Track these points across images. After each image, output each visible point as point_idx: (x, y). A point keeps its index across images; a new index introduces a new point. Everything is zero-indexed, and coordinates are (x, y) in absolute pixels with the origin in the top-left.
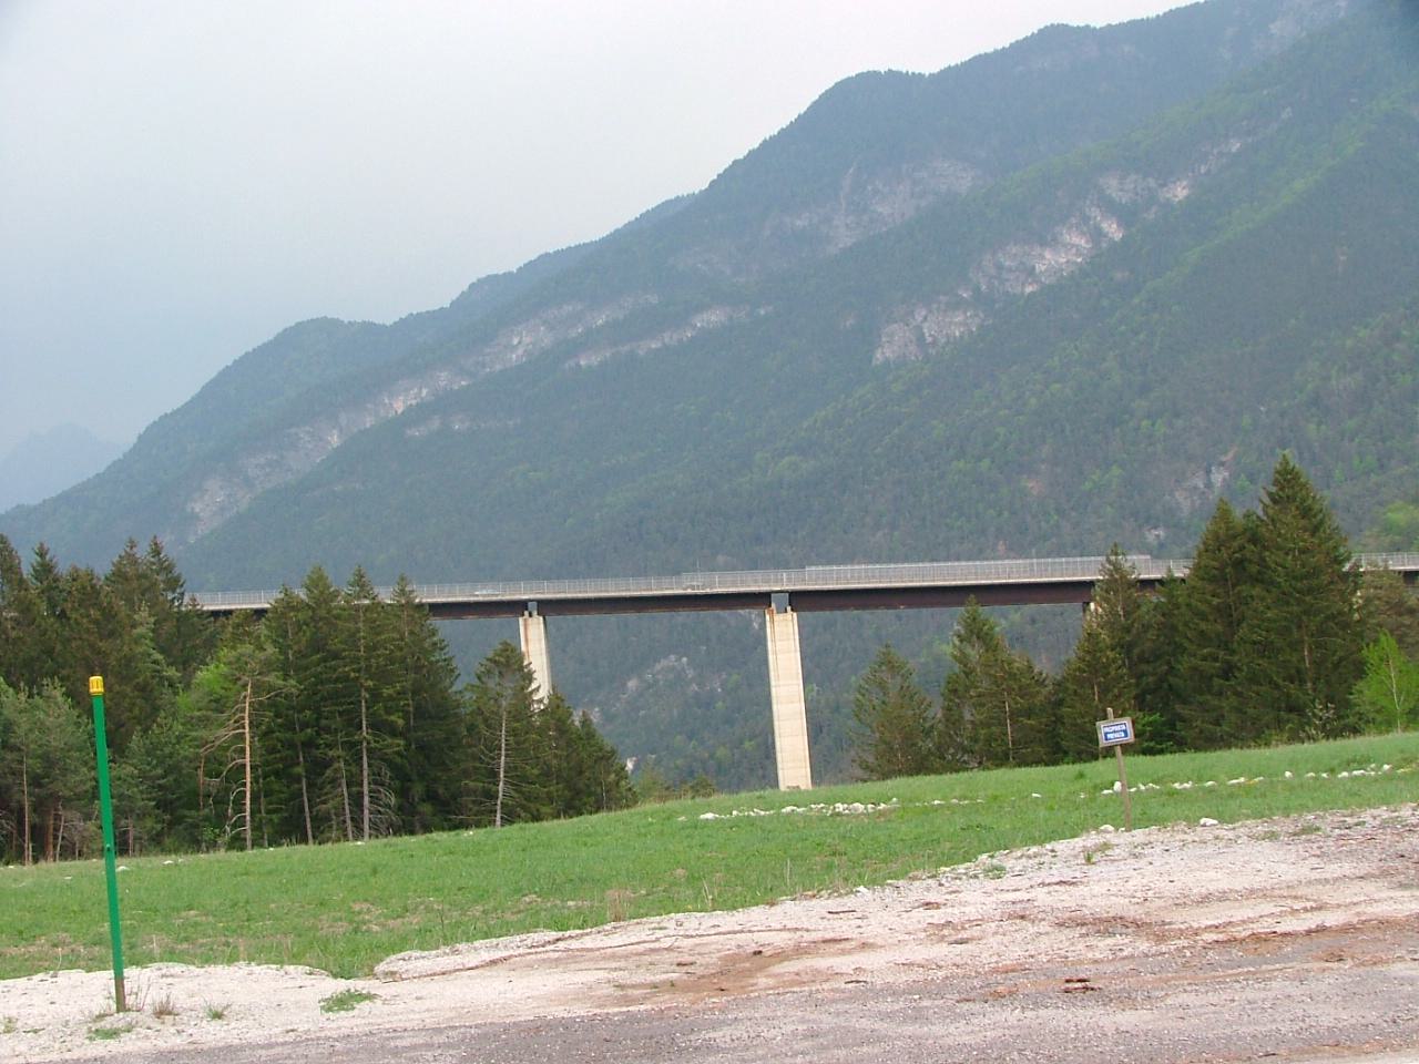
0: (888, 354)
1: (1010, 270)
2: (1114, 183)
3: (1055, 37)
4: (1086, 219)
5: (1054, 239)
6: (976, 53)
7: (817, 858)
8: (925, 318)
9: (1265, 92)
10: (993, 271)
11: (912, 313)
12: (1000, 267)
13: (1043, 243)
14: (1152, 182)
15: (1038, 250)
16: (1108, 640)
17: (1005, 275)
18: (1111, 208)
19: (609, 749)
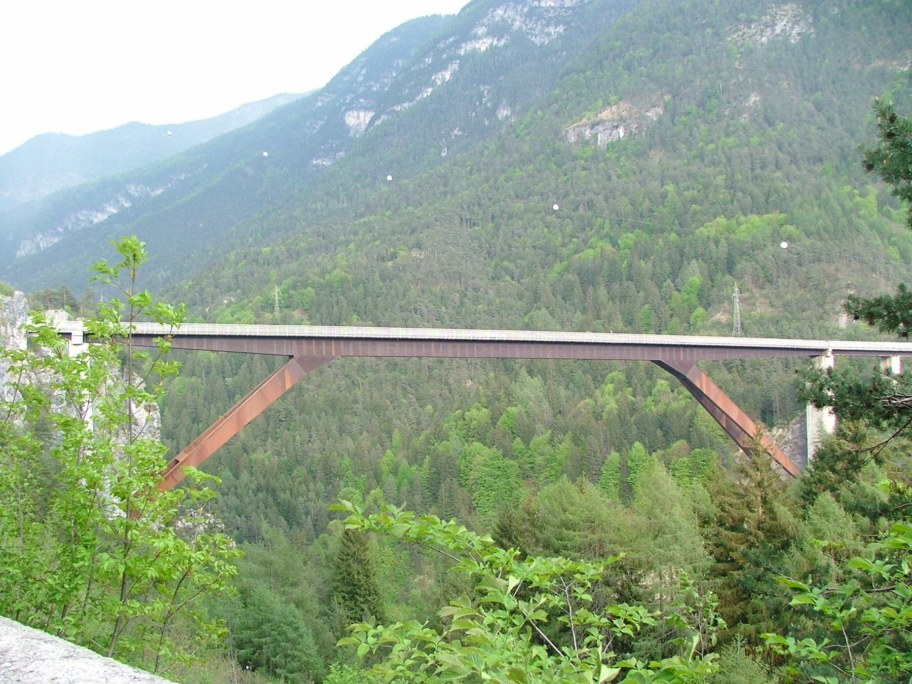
0: (23, 253)
1: (82, 221)
2: (133, 188)
3: (133, 127)
4: (118, 202)
5: (103, 209)
6: (404, 19)
7: (685, 459)
8: (41, 239)
9: (412, 83)
10: (74, 221)
11: (35, 236)
12: (78, 219)
13: (98, 211)
14: (148, 189)
15: (95, 213)
16: (691, 279)
17: (79, 223)
18: (129, 197)
19: (749, 239)
